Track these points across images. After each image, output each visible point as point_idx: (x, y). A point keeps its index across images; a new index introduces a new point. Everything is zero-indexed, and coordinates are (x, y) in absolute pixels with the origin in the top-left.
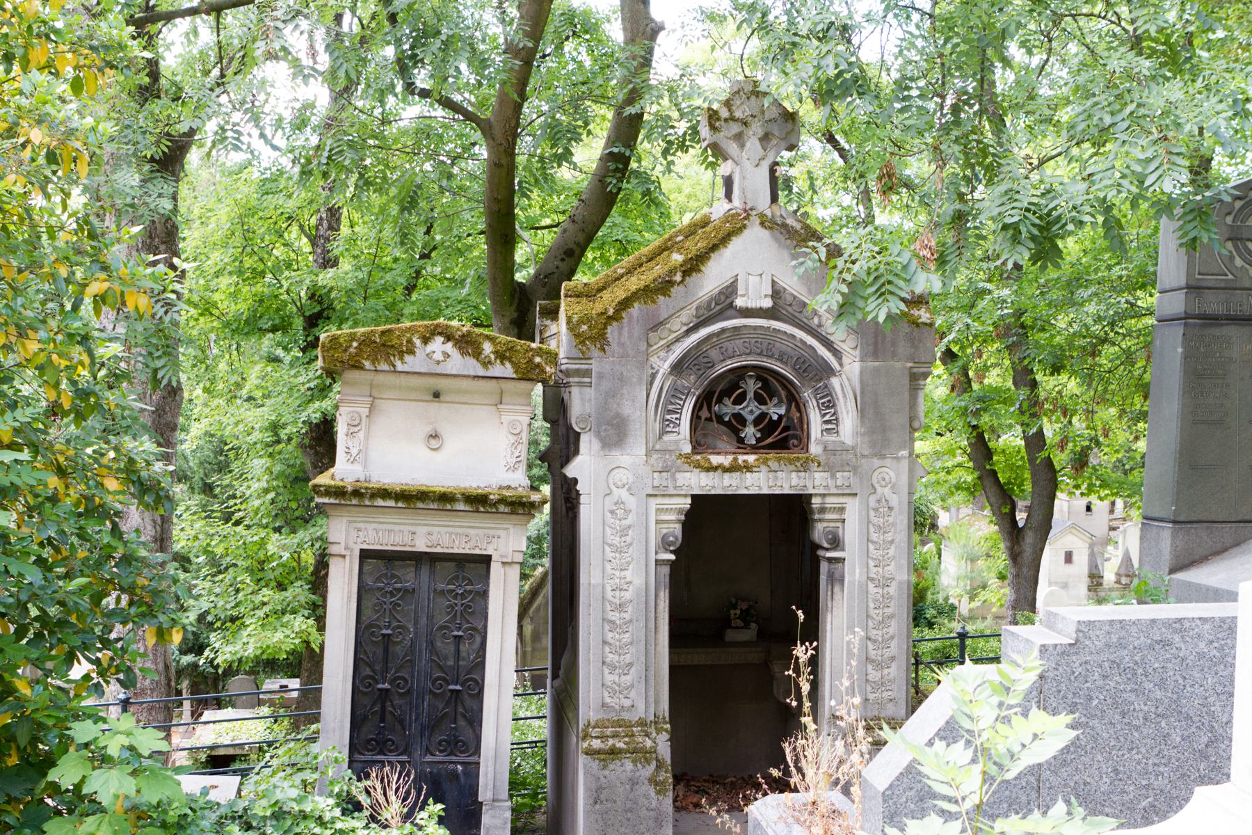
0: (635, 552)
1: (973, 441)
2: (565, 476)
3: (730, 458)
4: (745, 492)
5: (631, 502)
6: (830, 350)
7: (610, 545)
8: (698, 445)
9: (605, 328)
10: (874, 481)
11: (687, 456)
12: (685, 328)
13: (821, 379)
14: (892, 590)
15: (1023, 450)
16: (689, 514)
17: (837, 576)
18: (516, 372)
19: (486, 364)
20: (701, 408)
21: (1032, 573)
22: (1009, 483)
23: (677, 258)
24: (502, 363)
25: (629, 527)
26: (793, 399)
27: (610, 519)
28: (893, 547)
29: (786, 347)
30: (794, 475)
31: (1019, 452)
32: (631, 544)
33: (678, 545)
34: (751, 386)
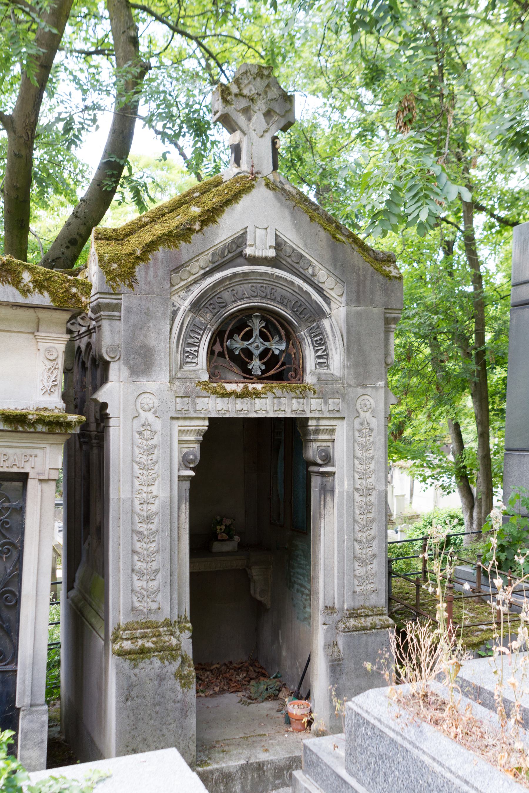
5: (157, 424)
7: (138, 463)
11: (205, 384)
12: (202, 272)
13: (314, 321)
14: (373, 498)
17: (328, 487)
18: (54, 301)
23: (195, 210)
24: (41, 292)
25: (155, 446)
27: (137, 439)
28: (373, 462)
30: (294, 401)
32: (156, 462)
34: (257, 325)
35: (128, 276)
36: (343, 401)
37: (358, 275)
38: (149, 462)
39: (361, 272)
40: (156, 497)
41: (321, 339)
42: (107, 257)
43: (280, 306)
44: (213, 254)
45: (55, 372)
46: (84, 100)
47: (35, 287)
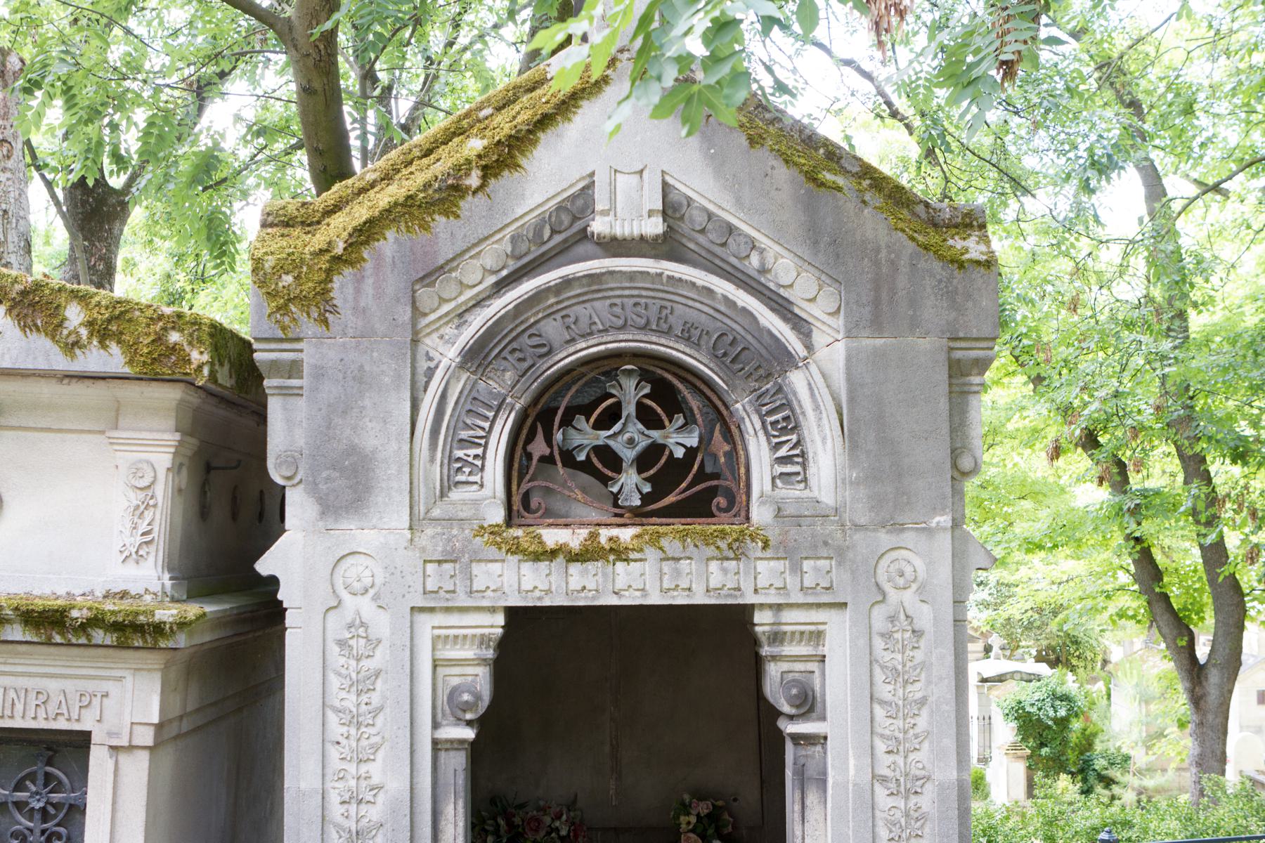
0: (391, 725)
1: (1137, 556)
2: (258, 575)
3: (584, 533)
4: (614, 601)
5: (381, 624)
6: (785, 319)
7: (338, 711)
8: (519, 507)
9: (328, 279)
10: (882, 577)
11: (494, 531)
12: (492, 279)
13: (769, 375)
14: (926, 801)
15: (1201, 567)
16: (504, 645)
17: (811, 771)
18: (130, 362)
19: (71, 347)
20: (530, 438)
21: (1218, 720)
22: (1185, 609)
23: (475, 145)
24: (103, 346)
25: (377, 674)
26: (721, 419)
27: (337, 658)
28: (925, 712)
29: (696, 313)
30: (714, 566)
31: (1195, 571)
32: (381, 709)
33: (481, 711)
34: (630, 392)
35: (319, 301)
36: (839, 564)
37: (877, 263)
38: (363, 708)
39: (883, 254)
40: (378, 788)
41: (786, 419)
42: (270, 262)
43: (682, 347)
44: (514, 240)
45: (148, 515)
46: (911, 50)
47: (91, 334)
